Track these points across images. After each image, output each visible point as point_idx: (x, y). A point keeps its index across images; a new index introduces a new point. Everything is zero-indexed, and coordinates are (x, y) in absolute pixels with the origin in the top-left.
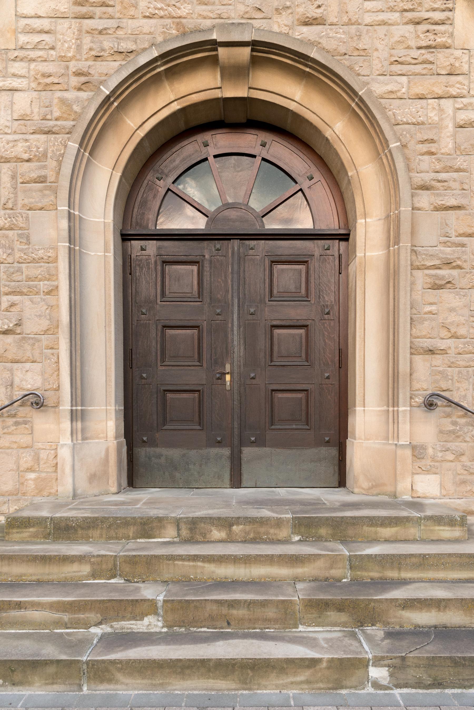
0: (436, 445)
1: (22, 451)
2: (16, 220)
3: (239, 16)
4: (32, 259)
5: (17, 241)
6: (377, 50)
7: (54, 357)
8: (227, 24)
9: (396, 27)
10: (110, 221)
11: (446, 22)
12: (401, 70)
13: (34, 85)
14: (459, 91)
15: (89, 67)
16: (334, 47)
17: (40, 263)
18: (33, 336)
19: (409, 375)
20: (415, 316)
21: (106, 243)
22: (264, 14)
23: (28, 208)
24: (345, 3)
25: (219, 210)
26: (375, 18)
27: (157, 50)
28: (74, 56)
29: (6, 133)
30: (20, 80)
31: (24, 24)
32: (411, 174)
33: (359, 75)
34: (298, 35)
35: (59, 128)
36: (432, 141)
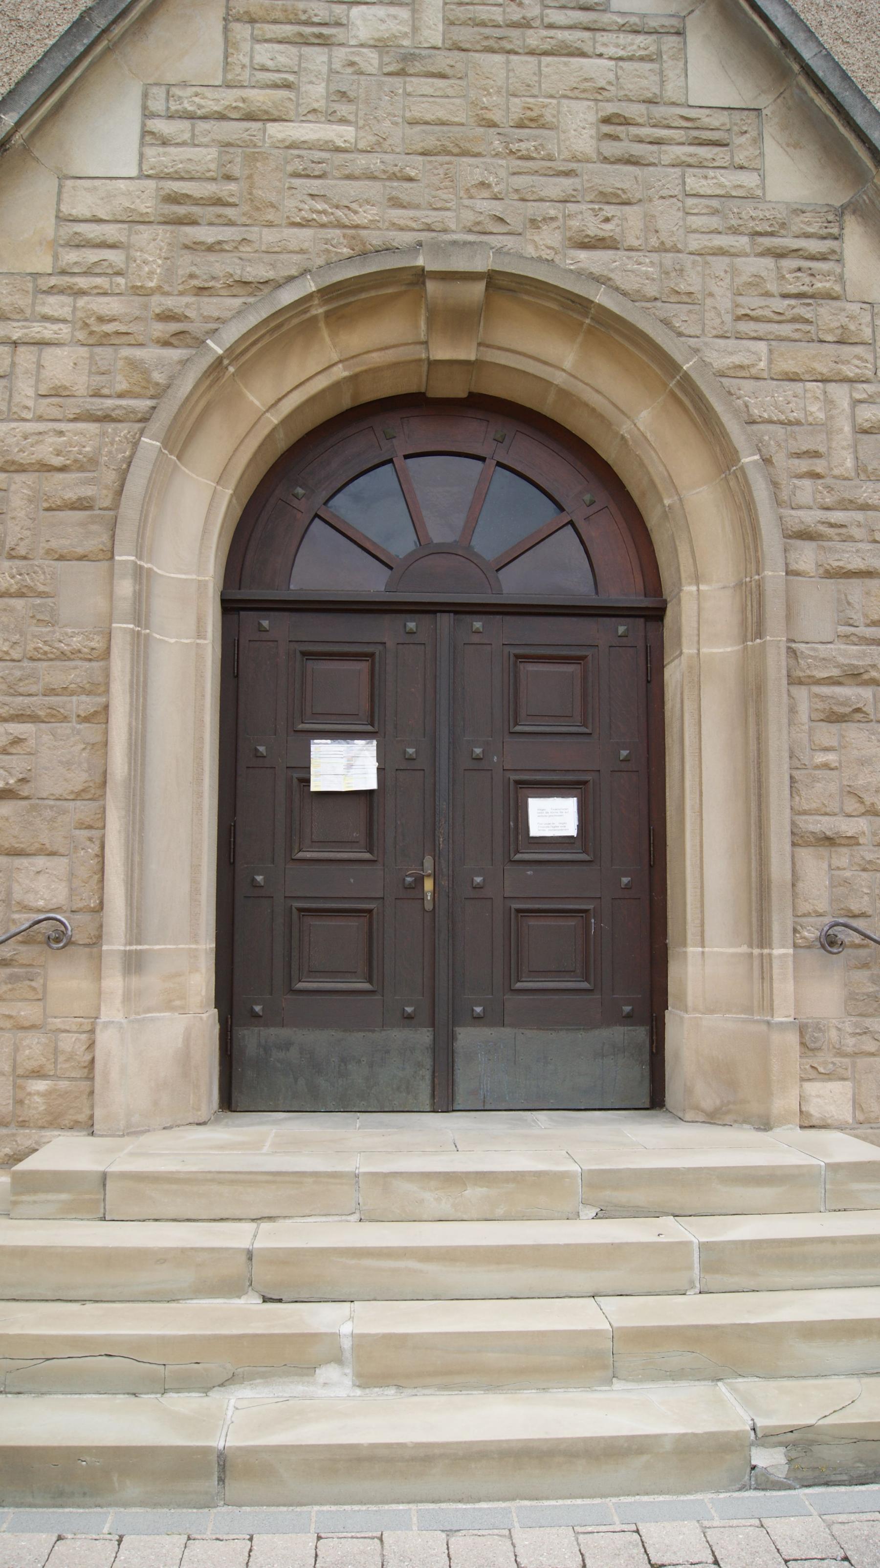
0: (844, 1022)
1: (21, 1034)
2: (32, 579)
3: (465, 228)
4: (59, 653)
5: (33, 617)
6: (711, 295)
7: (93, 845)
8: (444, 242)
9: (744, 259)
10: (207, 578)
11: (830, 257)
12: (756, 331)
13: (81, 335)
14: (857, 371)
15: (187, 305)
16: (636, 286)
17: (73, 660)
18: (52, 803)
19: (790, 886)
20: (798, 772)
21: (200, 621)
22: (510, 227)
23: (57, 556)
24: (654, 216)
25: (413, 558)
26: (706, 243)
27: (314, 281)
28: (159, 288)
29: (24, 420)
30: (55, 327)
31: (71, 232)
32: (782, 510)
33: (680, 334)
34: (571, 264)
35: (124, 412)
36: (816, 455)
